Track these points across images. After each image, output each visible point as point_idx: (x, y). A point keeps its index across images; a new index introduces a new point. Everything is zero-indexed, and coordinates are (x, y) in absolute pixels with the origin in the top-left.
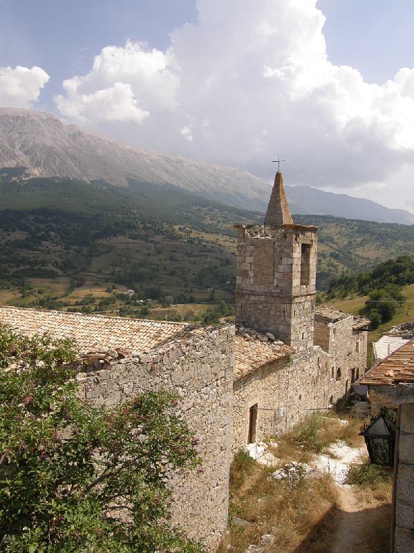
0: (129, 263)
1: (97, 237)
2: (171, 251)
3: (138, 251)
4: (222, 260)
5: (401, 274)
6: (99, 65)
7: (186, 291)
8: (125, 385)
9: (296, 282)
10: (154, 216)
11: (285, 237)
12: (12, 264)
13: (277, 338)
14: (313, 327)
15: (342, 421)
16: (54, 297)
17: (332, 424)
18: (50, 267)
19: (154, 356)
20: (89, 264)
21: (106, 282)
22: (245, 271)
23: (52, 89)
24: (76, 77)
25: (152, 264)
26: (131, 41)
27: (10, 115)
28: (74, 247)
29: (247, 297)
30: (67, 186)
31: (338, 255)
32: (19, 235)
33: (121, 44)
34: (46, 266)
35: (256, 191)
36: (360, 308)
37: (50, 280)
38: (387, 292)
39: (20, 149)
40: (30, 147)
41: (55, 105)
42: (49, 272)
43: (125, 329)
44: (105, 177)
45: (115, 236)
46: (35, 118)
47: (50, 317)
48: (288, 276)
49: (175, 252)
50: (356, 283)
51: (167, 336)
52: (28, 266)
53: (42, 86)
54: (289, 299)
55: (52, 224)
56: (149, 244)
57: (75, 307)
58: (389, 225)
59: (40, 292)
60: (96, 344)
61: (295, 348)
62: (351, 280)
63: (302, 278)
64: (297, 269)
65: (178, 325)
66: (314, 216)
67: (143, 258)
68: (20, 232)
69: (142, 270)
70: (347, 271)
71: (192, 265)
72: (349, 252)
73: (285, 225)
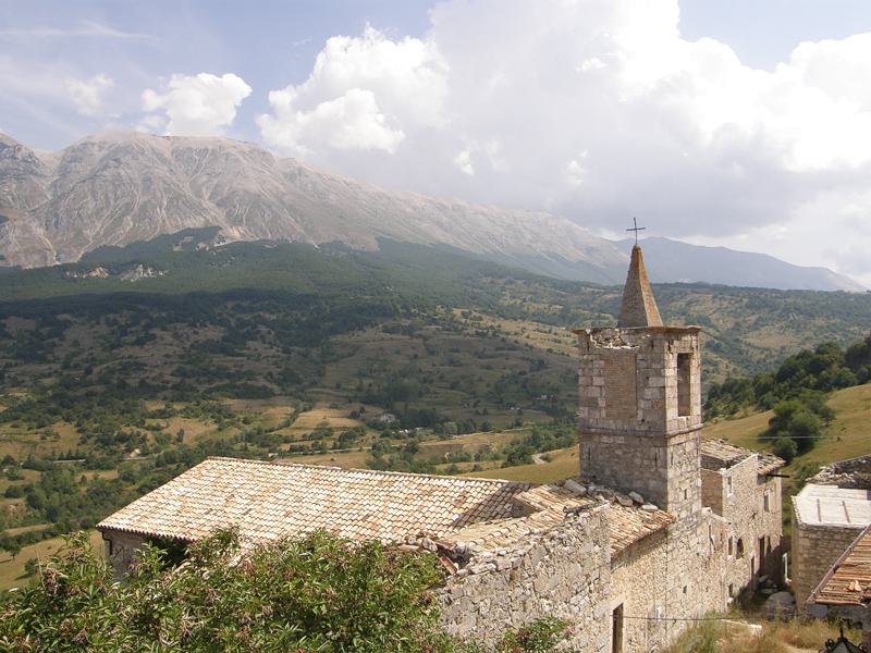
0: (385, 370)
1: (333, 331)
2: (452, 351)
3: (397, 352)
4: (532, 361)
5: (824, 372)
6: (321, 67)
7: (477, 413)
8: (482, 603)
9: (672, 413)
10: (421, 296)
11: (653, 346)
12: (202, 379)
13: (647, 500)
14: (700, 480)
15: (753, 626)
16: (268, 428)
17: (737, 631)
18: (262, 382)
19: (513, 559)
20: (321, 374)
21: (350, 401)
22: (592, 398)
23: (251, 109)
24: (290, 87)
25: (420, 371)
26: (371, 25)
27: (194, 147)
28: (297, 348)
29: (596, 439)
30: (283, 254)
31: (718, 346)
32: (213, 333)
33: (355, 31)
34: (256, 380)
35: (581, 249)
36: (760, 431)
37: (262, 401)
38: (804, 402)
39: (210, 199)
40: (225, 195)
41: (257, 129)
42: (259, 389)
43: (410, 491)
44: (342, 238)
45: (360, 329)
46: (233, 151)
47: (293, 474)
48: (660, 406)
49: (457, 351)
50: (751, 390)
51: (475, 501)
52: (227, 381)
53: (238, 104)
54: (663, 439)
55: (262, 313)
56: (415, 340)
57: (302, 444)
58: (799, 293)
59: (246, 422)
60: (368, 516)
61: (675, 514)
62: (743, 385)
63: (680, 404)
64: (672, 394)
65: (491, 483)
66: (677, 284)
67: (407, 362)
68: (211, 327)
69: (406, 381)
70: (734, 370)
71: (485, 371)
72: (737, 340)
73: (652, 329)
